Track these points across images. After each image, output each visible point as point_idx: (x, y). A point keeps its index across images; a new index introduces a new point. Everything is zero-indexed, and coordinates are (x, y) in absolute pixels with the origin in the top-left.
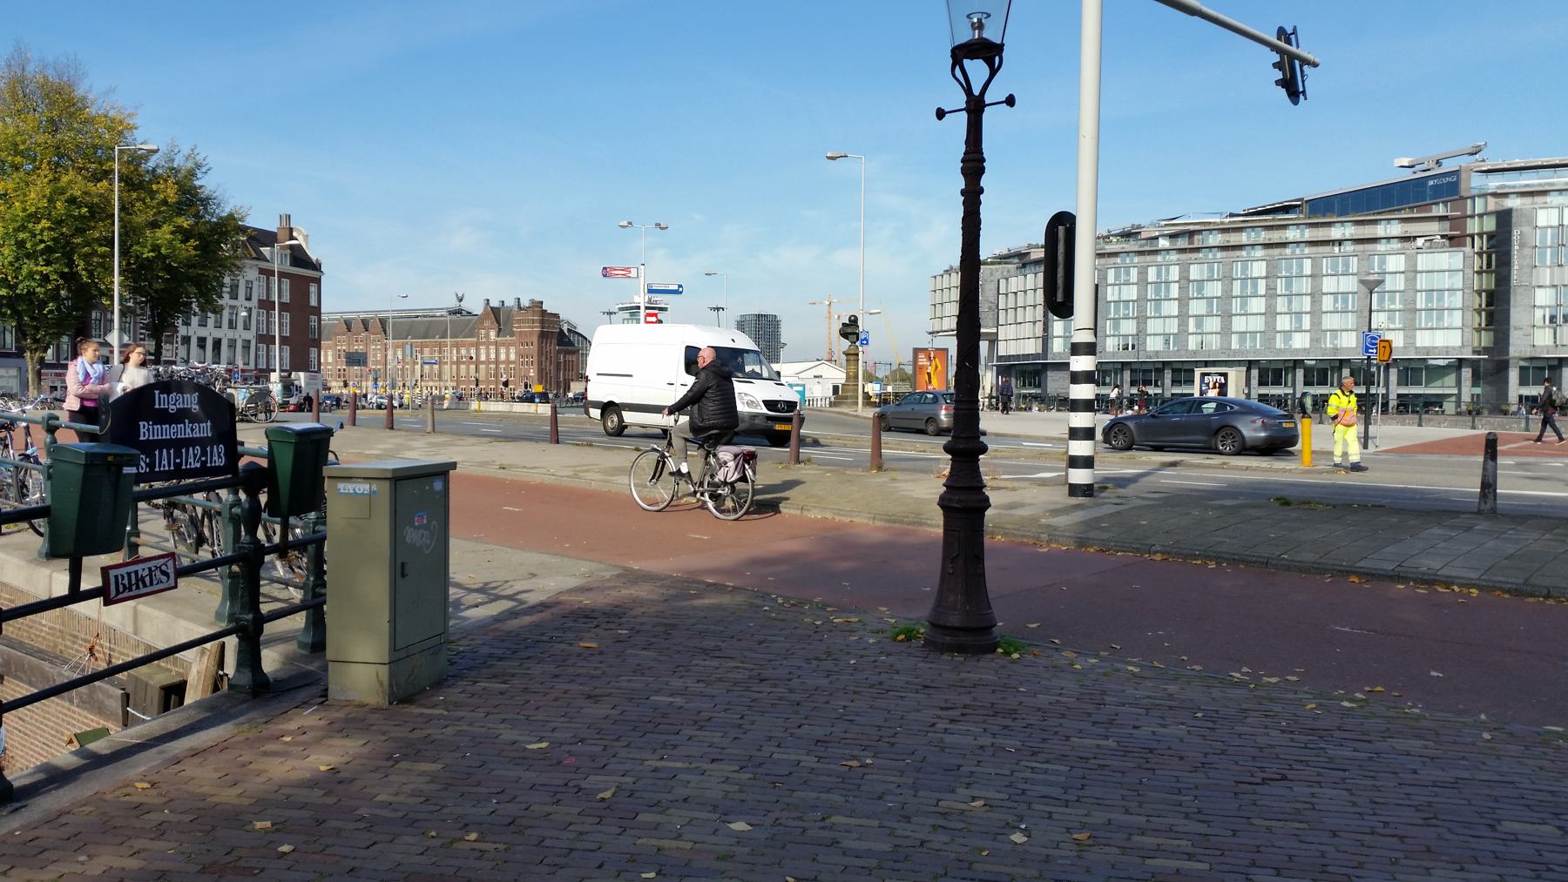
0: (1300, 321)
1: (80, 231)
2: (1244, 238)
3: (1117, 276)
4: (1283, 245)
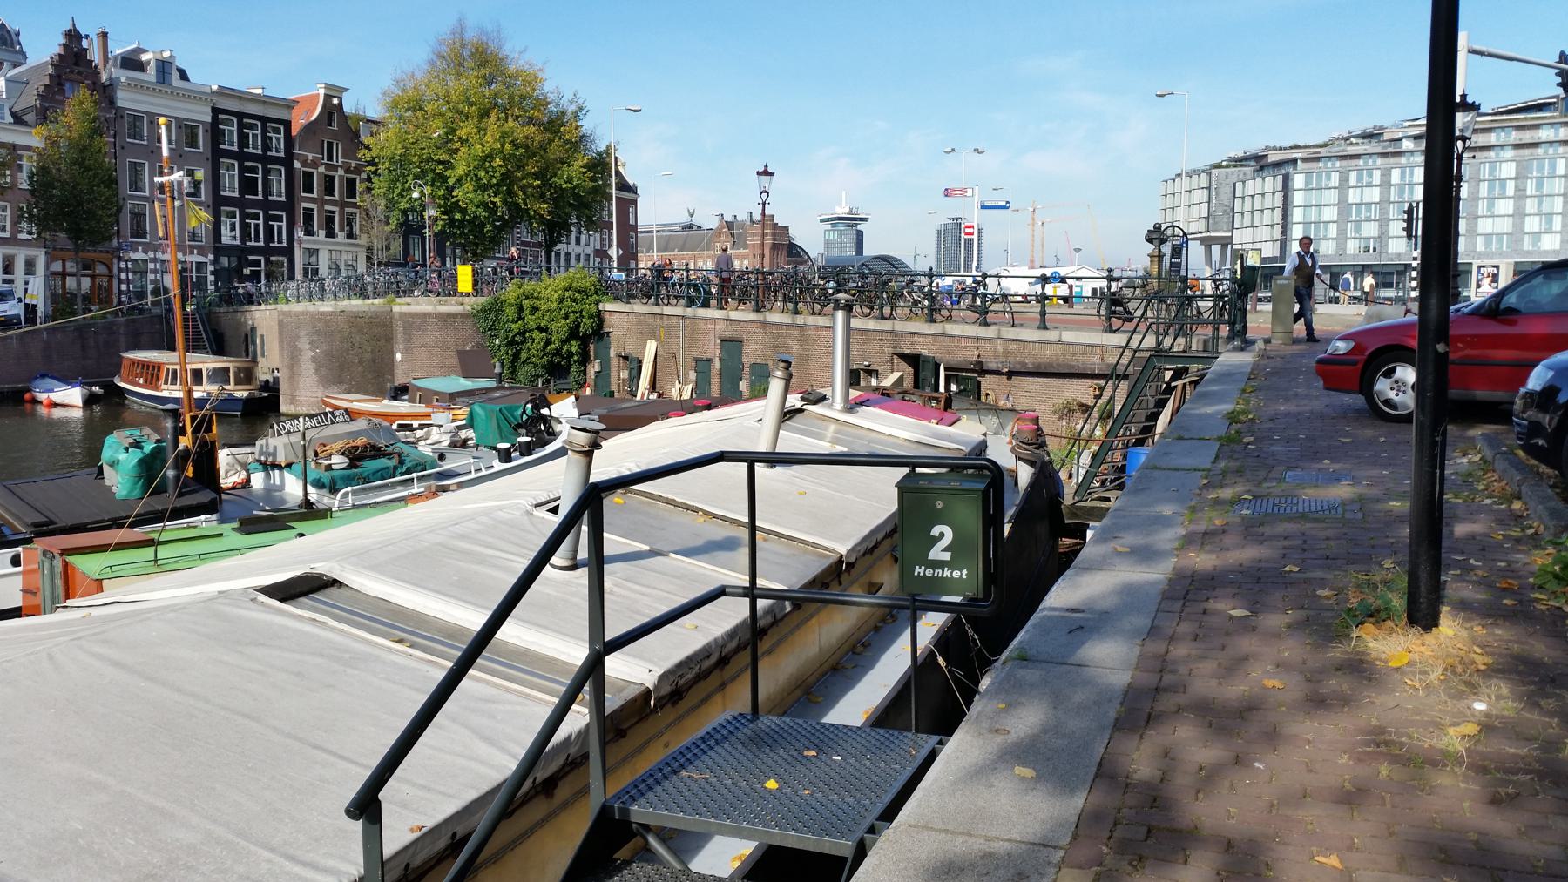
0: (1550, 222)
1: (520, 167)
2: (1492, 139)
3: (1359, 179)
4: (1535, 145)
